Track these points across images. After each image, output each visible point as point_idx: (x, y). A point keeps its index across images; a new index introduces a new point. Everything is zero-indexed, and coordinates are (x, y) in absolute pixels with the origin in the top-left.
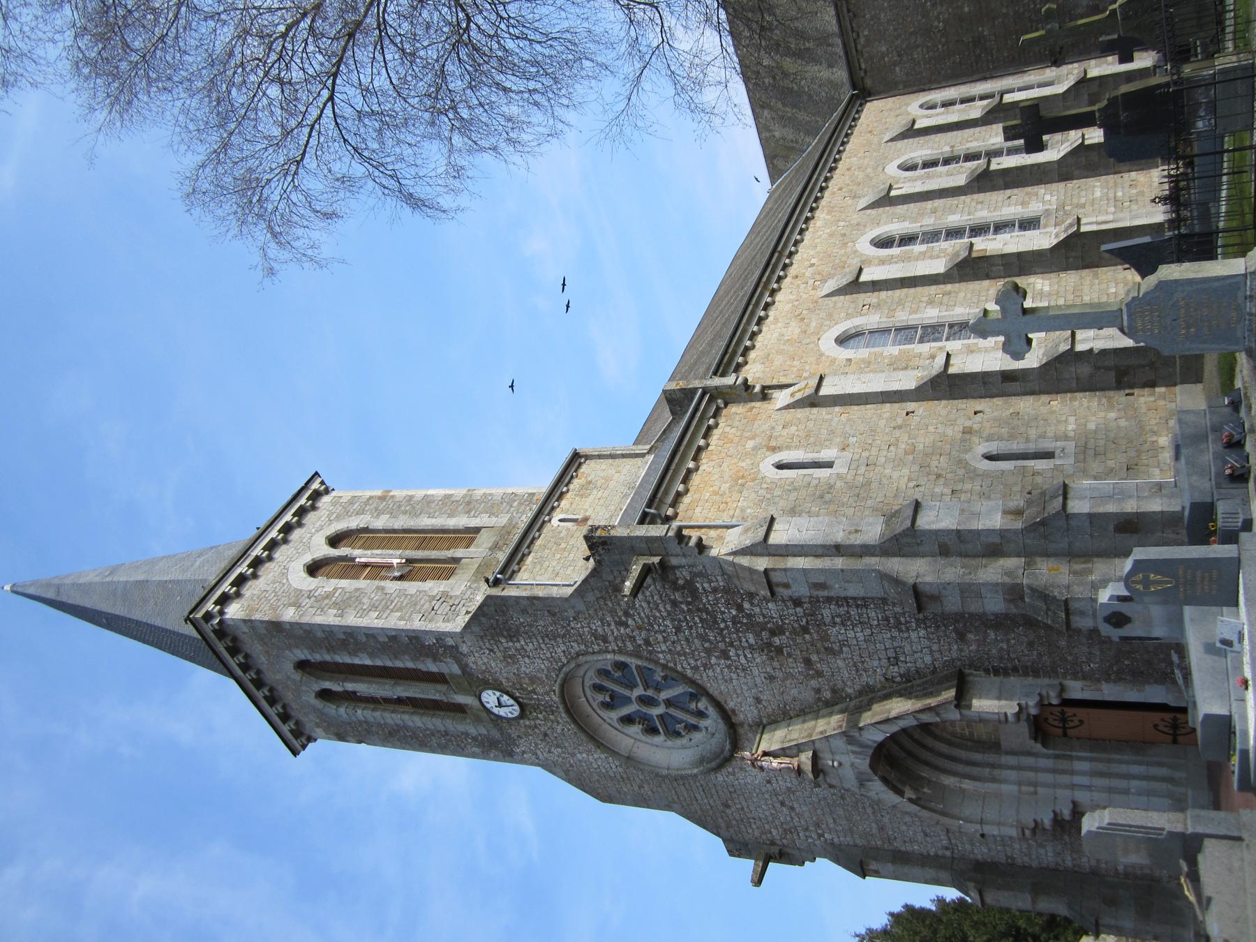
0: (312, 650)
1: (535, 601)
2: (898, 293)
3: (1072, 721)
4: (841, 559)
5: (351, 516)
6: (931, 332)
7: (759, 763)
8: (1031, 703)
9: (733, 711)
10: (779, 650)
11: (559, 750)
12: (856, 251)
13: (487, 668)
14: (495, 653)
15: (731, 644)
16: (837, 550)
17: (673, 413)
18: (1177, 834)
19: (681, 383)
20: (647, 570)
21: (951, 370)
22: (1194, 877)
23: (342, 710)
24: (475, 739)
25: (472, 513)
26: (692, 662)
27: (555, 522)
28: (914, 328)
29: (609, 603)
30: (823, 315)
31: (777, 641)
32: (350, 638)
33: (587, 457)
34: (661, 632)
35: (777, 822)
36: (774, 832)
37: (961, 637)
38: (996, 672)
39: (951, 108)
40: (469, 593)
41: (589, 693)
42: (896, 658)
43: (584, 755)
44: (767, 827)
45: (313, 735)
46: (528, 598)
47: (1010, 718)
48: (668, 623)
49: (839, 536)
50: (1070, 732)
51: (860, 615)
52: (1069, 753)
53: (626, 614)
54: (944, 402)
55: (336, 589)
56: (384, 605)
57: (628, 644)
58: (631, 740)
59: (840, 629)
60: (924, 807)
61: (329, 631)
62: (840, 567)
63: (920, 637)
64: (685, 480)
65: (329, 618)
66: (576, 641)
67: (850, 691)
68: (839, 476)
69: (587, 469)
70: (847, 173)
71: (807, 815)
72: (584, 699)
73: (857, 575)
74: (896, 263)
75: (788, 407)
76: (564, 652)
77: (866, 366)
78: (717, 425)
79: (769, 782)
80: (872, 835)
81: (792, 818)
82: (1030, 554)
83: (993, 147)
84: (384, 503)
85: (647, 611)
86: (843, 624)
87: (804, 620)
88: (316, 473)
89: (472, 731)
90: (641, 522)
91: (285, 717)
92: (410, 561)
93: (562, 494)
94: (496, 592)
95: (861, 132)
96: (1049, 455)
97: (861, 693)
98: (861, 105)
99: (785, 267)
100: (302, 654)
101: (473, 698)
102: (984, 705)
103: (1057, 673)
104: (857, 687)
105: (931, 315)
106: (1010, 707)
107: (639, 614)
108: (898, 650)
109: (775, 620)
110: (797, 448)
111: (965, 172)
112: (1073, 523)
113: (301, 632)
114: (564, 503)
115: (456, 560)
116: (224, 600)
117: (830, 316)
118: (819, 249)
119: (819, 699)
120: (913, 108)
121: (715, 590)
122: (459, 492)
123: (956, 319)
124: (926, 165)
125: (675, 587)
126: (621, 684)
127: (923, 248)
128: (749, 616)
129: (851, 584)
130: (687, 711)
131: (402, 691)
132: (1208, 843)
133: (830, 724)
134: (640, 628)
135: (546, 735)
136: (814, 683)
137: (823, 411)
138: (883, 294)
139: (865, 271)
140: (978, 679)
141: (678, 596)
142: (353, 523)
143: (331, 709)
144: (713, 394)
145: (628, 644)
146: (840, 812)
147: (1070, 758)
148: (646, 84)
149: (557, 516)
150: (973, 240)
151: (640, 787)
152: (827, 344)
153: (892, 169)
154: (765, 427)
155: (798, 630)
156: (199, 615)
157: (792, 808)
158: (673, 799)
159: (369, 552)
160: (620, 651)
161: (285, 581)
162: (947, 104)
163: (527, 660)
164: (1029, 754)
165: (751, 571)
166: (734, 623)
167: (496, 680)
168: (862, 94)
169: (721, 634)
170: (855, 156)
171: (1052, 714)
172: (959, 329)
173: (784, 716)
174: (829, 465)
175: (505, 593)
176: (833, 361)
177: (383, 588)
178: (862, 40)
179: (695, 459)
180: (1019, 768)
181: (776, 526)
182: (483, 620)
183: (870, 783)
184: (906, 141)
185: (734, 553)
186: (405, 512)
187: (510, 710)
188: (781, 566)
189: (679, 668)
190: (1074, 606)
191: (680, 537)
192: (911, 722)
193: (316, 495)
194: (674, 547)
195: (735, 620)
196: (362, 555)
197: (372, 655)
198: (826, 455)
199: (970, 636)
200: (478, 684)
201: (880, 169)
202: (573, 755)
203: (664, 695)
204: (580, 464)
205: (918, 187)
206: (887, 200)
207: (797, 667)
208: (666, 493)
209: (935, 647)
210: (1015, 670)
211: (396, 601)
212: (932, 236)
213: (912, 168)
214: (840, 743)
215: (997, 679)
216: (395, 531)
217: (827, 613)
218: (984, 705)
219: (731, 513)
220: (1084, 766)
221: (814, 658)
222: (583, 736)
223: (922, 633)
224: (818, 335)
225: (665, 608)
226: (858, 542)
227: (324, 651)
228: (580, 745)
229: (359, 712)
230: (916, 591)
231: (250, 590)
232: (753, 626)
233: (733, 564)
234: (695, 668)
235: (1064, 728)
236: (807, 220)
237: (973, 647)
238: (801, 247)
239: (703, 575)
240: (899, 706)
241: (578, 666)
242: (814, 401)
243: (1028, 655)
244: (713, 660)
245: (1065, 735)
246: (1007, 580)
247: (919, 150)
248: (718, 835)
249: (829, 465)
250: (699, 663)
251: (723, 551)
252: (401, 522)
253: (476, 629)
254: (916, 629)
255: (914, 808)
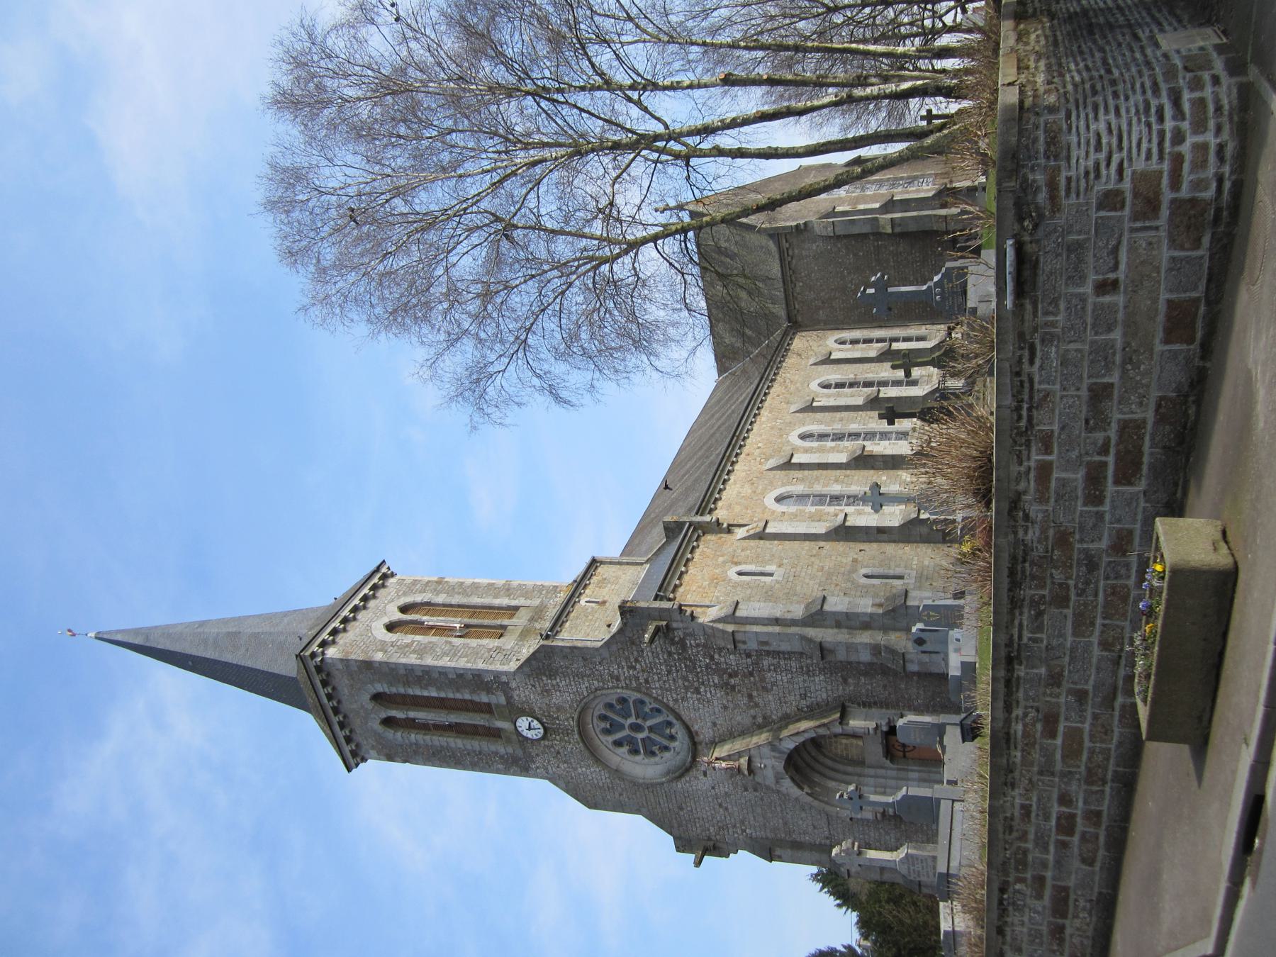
0: (391, 684)
2: (816, 473)
6: (836, 499)
8: (884, 723)
9: (697, 733)
10: (733, 688)
15: (703, 683)
16: (777, 621)
17: (667, 536)
21: (848, 524)
22: (941, 742)
23: (399, 734)
24: (502, 757)
26: (674, 696)
27: (583, 602)
28: (825, 496)
31: (732, 681)
32: (425, 675)
33: (602, 563)
34: (657, 674)
35: (715, 821)
36: (712, 829)
37: (845, 681)
38: (864, 705)
39: (856, 346)
41: (595, 720)
42: (805, 695)
44: (707, 825)
45: (366, 756)
46: (570, 647)
47: (871, 731)
48: (663, 667)
49: (778, 614)
50: (907, 754)
51: (786, 665)
54: (842, 543)
56: (454, 652)
57: (633, 682)
58: (620, 758)
60: (816, 799)
61: (410, 669)
65: (412, 660)
66: (597, 680)
67: (774, 717)
68: (777, 582)
69: (601, 569)
71: (736, 814)
73: (789, 637)
75: (745, 538)
77: (794, 517)
78: (698, 546)
79: (713, 788)
82: (885, 629)
85: (651, 659)
86: (775, 670)
89: (502, 751)
90: (655, 599)
91: (349, 740)
92: (467, 626)
93: (586, 585)
96: (901, 577)
97: (781, 719)
98: (794, 334)
99: (741, 446)
100: (379, 688)
102: (856, 723)
103: (899, 706)
104: (779, 715)
105: (836, 489)
106: (872, 725)
110: (751, 563)
112: (910, 611)
114: (587, 591)
115: (504, 627)
116: (324, 644)
117: (771, 483)
120: (830, 342)
121: (698, 645)
122: (500, 582)
123: (852, 493)
125: (673, 642)
126: (619, 715)
127: (833, 444)
128: (717, 664)
130: (662, 736)
131: (454, 718)
132: (948, 727)
133: (762, 738)
134: (643, 671)
135: (558, 753)
136: (752, 712)
137: (767, 543)
138: (806, 472)
139: (795, 456)
140: (853, 709)
141: (673, 649)
142: (419, 598)
143: (390, 734)
144: (696, 527)
145: (633, 682)
146: (759, 810)
147: (907, 770)
148: (698, 353)
150: (866, 443)
151: (621, 795)
152: (769, 500)
153: (814, 386)
154: (731, 550)
156: (308, 653)
157: (727, 809)
159: (435, 618)
160: (627, 687)
162: (854, 342)
164: (882, 767)
165: (724, 632)
166: (707, 668)
168: (795, 325)
169: (697, 676)
172: (853, 499)
173: (731, 735)
174: (771, 575)
176: (774, 512)
177: (450, 643)
178: (798, 289)
180: (876, 776)
181: (740, 606)
182: (534, 662)
185: (713, 621)
186: (459, 593)
187: (536, 734)
188: (742, 629)
189: (665, 700)
190: (907, 657)
191: (680, 609)
192: (812, 734)
193: (385, 577)
194: (676, 616)
195: (707, 666)
196: (428, 620)
198: (769, 568)
199: (850, 680)
200: (515, 711)
202: (575, 769)
203: (649, 723)
204: (597, 567)
206: (810, 408)
208: (669, 584)
209: (829, 688)
210: (875, 703)
212: (839, 437)
214: (766, 751)
215: (865, 710)
216: (451, 606)
217: (766, 662)
218: (856, 723)
220: (915, 775)
221: (755, 694)
222: (587, 753)
223: (822, 678)
224: (763, 493)
229: (413, 736)
230: (821, 647)
231: (341, 639)
232: (719, 671)
233: (713, 628)
234: (676, 701)
235: (904, 752)
236: (756, 415)
237: (852, 688)
238: (751, 434)
239: (692, 635)
240: (804, 725)
241: (595, 697)
242: (761, 536)
245: (904, 756)
247: (834, 374)
248: (671, 834)
249: (771, 575)
252: (456, 600)
255: (810, 799)
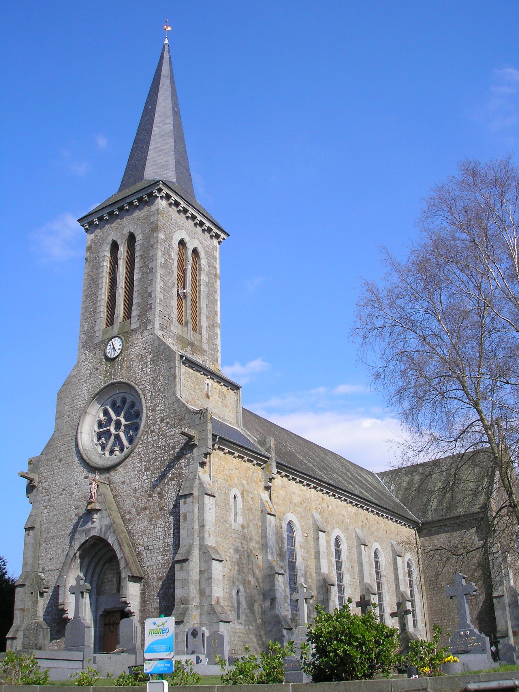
1: (173, 377)
3: (113, 628)
4: (198, 528)
5: (207, 259)
7: (94, 483)
10: (150, 496)
11: (88, 375)
12: (334, 528)
13: (135, 344)
14: (144, 350)
15: (153, 473)
18: (136, 647)
19: (274, 446)
20: (191, 438)
25: (208, 329)
27: (208, 381)
29: (173, 415)
30: (303, 513)
34: (159, 439)
39: (407, 575)
40: (172, 334)
41: (122, 395)
43: (86, 388)
48: (163, 443)
52: (98, 626)
53: (168, 423)
55: (172, 259)
57: (151, 422)
59: (162, 525)
61: (153, 258)
62: (195, 527)
63: (159, 560)
64: (229, 452)
65: (160, 260)
70: (376, 522)
72: (118, 392)
74: (327, 549)
76: (146, 387)
79: (76, 484)
80: (48, 533)
81: (56, 493)
82: (200, 607)
83: (384, 597)
84: (213, 277)
85: (170, 434)
86: (165, 526)
87: (167, 509)
88: (229, 235)
94: (177, 358)
95: (397, 528)
101: (117, 333)
107: (168, 429)
108: (153, 551)
109: (166, 495)
111: (371, 582)
113: (152, 243)
118: (336, 510)
119: (125, 513)
124: (377, 563)
127: (334, 562)
129: (186, 531)
132: (134, 656)
135: (97, 369)
142: (203, 261)
145: (151, 422)
146: (62, 518)
149: (210, 381)
150: (336, 586)
155: (162, 506)
157: (61, 494)
158: (62, 432)
161: (176, 229)
163: (140, 366)
165: (192, 487)
167: (128, 347)
170: (385, 526)
171: (117, 618)
175: (177, 361)
177: (174, 287)
179: (239, 457)
183: (84, 535)
184: (391, 552)
185: (199, 479)
189: (139, 446)
197: (140, 280)
201: (376, 540)
205: (365, 560)
207: (142, 504)
209: (154, 567)
211: (168, 295)
213: (376, 556)
219: (216, 476)
221: (147, 512)
223: (162, 562)
224: (295, 512)
225: (171, 443)
226: (205, 535)
227: (142, 253)
228: (92, 386)
235: (109, 624)
243: (152, 607)
244: (144, 463)
246: (190, 598)
249: (235, 520)
250: (142, 456)
251: (200, 473)
252: (203, 288)
253: (156, 343)
254: (163, 559)
